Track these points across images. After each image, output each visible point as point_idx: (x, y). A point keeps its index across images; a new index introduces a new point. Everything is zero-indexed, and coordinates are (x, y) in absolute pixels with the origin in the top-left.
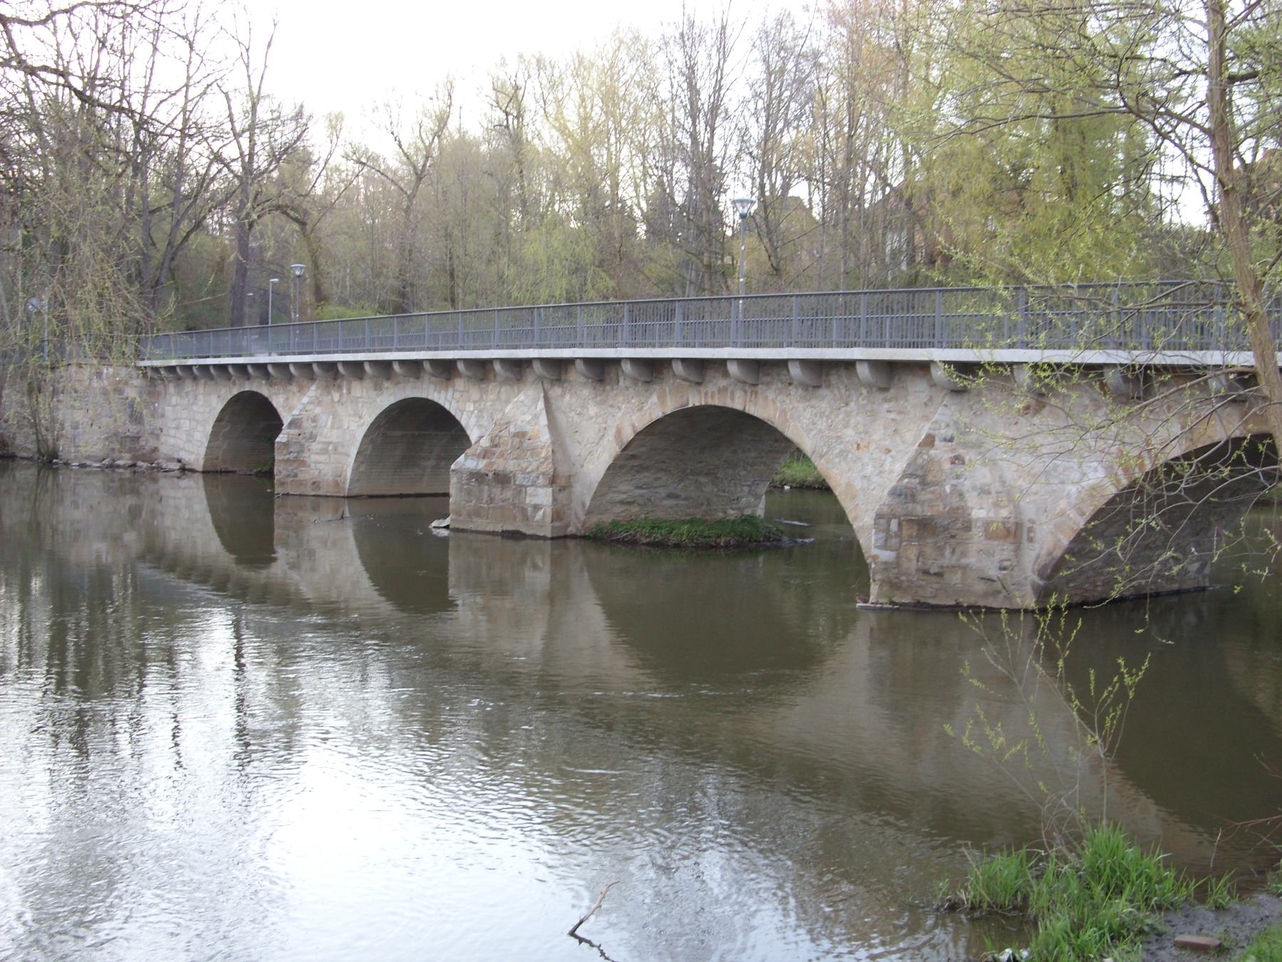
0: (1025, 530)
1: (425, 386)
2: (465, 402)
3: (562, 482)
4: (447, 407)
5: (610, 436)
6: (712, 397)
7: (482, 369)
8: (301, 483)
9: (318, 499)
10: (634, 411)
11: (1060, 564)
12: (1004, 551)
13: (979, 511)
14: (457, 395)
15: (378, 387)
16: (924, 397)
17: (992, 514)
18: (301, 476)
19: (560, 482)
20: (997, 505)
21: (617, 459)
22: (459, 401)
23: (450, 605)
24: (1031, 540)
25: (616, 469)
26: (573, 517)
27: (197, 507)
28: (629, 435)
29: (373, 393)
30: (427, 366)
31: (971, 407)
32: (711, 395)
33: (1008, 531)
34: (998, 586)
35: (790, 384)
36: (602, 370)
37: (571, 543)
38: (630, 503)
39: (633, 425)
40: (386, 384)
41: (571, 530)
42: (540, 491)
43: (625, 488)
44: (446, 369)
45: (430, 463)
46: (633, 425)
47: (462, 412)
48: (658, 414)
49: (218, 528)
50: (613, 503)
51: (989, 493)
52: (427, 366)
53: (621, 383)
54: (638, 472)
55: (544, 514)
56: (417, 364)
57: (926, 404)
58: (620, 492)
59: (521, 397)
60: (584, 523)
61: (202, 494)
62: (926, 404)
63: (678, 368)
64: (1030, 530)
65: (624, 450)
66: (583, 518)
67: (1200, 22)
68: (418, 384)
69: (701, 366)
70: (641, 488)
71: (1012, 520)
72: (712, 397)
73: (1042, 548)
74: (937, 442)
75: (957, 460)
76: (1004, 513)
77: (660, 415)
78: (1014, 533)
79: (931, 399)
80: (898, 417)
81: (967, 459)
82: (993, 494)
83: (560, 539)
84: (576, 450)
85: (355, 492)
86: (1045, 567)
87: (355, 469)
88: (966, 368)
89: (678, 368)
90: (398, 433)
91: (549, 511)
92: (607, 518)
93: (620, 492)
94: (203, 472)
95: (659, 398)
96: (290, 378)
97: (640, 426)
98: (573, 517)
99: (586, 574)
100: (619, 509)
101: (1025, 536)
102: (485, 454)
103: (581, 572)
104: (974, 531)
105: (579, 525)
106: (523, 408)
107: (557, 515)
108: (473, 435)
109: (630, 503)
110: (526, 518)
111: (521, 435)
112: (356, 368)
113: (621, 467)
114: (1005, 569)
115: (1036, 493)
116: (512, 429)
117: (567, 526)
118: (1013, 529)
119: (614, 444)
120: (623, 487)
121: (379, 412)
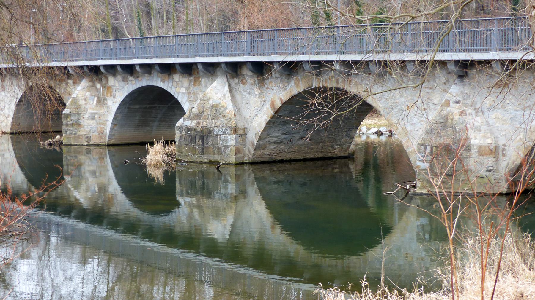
0: (501, 150)
1: (155, 78)
2: (180, 88)
3: (241, 132)
4: (169, 91)
5: (268, 105)
6: (326, 82)
7: (188, 69)
8: (79, 137)
9: (90, 147)
10: (279, 92)
11: (519, 167)
12: (489, 161)
13: (476, 140)
14: (175, 84)
15: (125, 80)
16: (443, 80)
17: (482, 142)
18: (79, 134)
19: (240, 133)
20: (485, 137)
21: (272, 117)
22: (178, 88)
23: (177, 204)
24: (504, 155)
25: (271, 123)
26: (247, 152)
27: (7, 155)
28: (278, 104)
29: (122, 84)
30: (119, 68)
31: (470, 84)
32: (329, 81)
33: (491, 150)
34: (486, 180)
35: (370, 74)
36: (260, 69)
37: (246, 167)
38: (279, 143)
39: (281, 99)
40: (131, 78)
41: (246, 159)
42: (229, 137)
43: (276, 134)
44: (168, 69)
45: (156, 123)
46: (281, 99)
47: (178, 93)
48: (295, 92)
49: (21, 167)
50: (270, 143)
51: (480, 131)
52: (119, 68)
53: (273, 75)
54: (284, 125)
55: (231, 150)
56: (113, 67)
57: (445, 84)
58: (273, 137)
59: (215, 84)
60: (254, 154)
61: (11, 147)
62: (445, 84)
63: (307, 67)
64: (504, 150)
65: (276, 113)
66: (253, 152)
67: (434, 57)
68: (150, 78)
69: (318, 65)
70: (285, 134)
71: (493, 145)
72: (326, 82)
73: (510, 159)
74: (451, 104)
75: (462, 113)
76: (489, 141)
77: (296, 93)
78: (495, 152)
79: (447, 81)
80: (430, 91)
81: (468, 112)
82: (483, 131)
83: (239, 164)
84: (246, 113)
85: (111, 142)
86: (512, 170)
87: (112, 129)
88: (347, 64)
89: (307, 67)
90: (137, 107)
91: (234, 148)
92: (267, 152)
93: (273, 137)
94: (12, 133)
95: (295, 83)
96: (69, 76)
97: (285, 99)
98: (247, 152)
99: (256, 186)
100: (273, 147)
101: (501, 153)
102: (198, 116)
103: (253, 184)
104: (473, 151)
105: (251, 156)
106: (217, 90)
107: (238, 151)
108: (186, 106)
109: (279, 143)
110: (220, 153)
111: (215, 106)
112: (111, 69)
113: (274, 123)
114: (490, 171)
115: (506, 130)
116: (211, 103)
117: (244, 157)
118: (494, 150)
119: (270, 110)
120: (275, 134)
121: (126, 94)
